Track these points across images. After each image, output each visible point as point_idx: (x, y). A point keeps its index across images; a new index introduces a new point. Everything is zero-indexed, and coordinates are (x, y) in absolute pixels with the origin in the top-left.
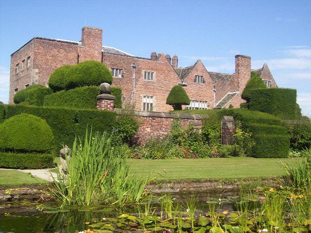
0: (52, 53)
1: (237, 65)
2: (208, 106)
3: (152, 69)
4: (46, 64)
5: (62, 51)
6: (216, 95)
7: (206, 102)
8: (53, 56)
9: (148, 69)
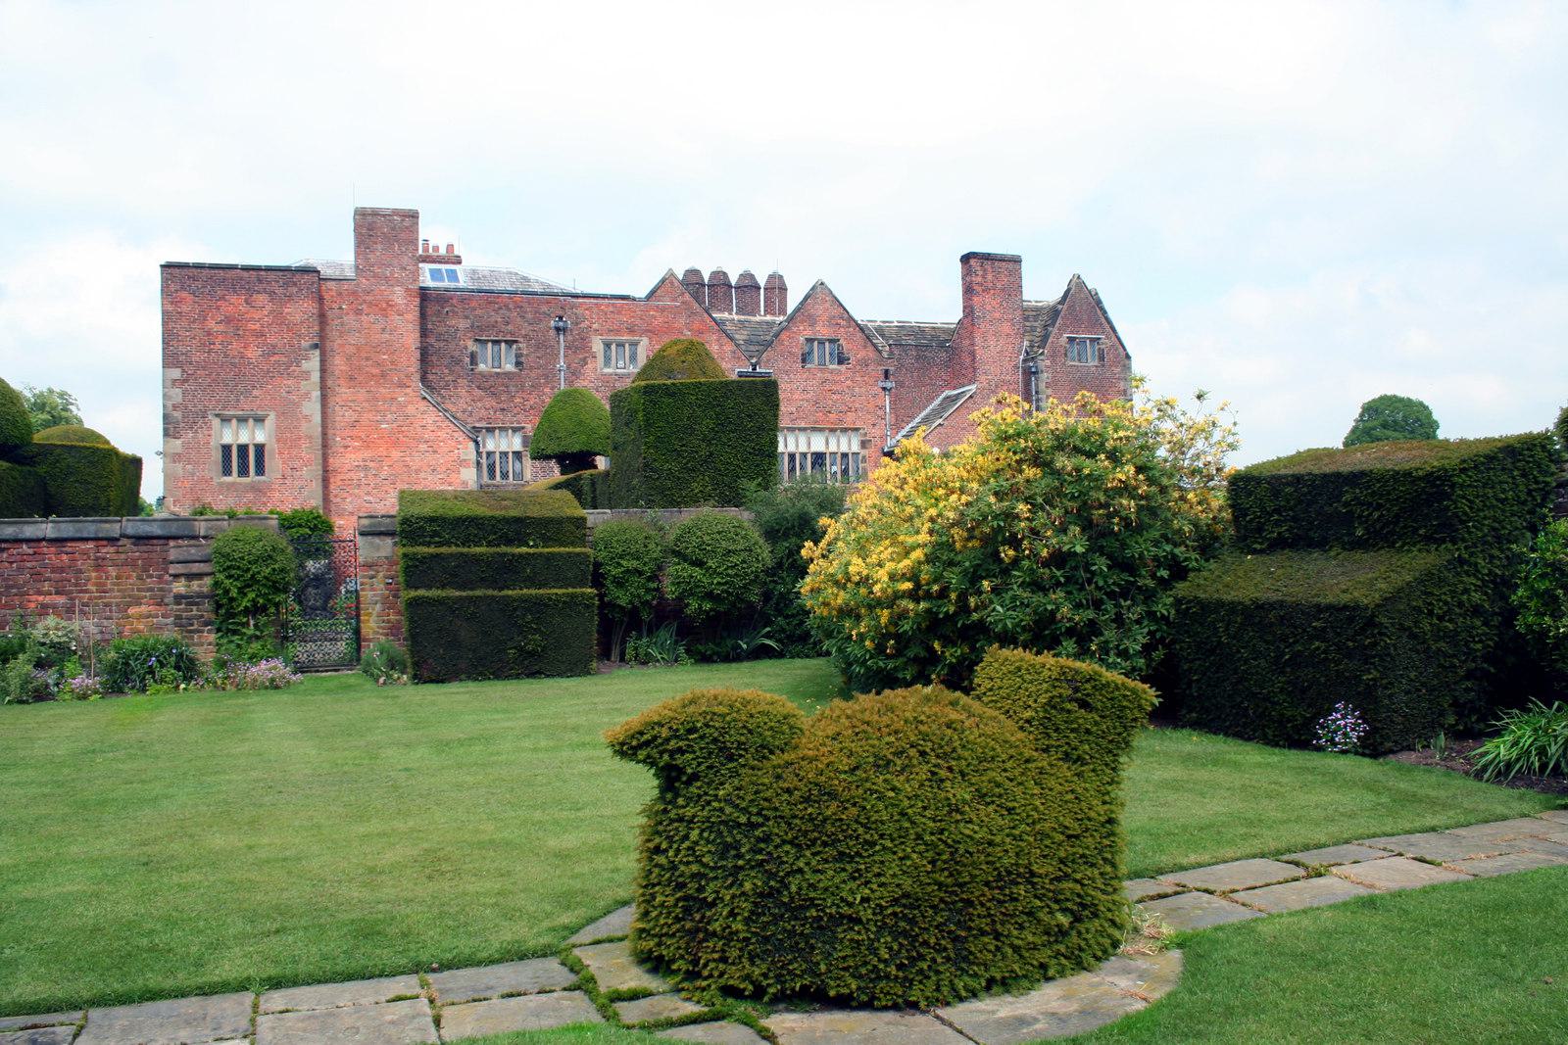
0: (226, 309)
1: (968, 291)
2: (864, 444)
3: (631, 331)
4: (207, 345)
5: (261, 299)
6: (893, 403)
7: (857, 429)
8: (228, 320)
9: (618, 332)
